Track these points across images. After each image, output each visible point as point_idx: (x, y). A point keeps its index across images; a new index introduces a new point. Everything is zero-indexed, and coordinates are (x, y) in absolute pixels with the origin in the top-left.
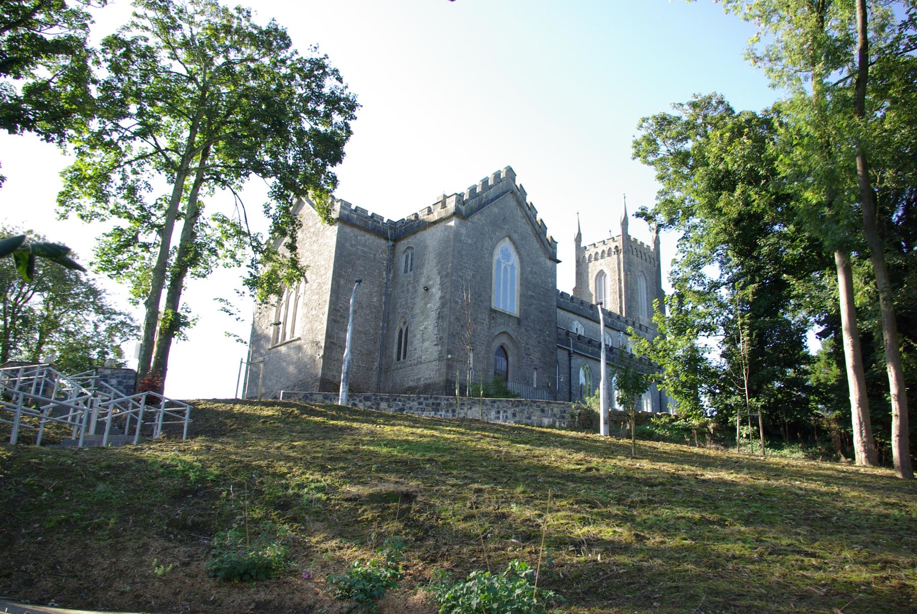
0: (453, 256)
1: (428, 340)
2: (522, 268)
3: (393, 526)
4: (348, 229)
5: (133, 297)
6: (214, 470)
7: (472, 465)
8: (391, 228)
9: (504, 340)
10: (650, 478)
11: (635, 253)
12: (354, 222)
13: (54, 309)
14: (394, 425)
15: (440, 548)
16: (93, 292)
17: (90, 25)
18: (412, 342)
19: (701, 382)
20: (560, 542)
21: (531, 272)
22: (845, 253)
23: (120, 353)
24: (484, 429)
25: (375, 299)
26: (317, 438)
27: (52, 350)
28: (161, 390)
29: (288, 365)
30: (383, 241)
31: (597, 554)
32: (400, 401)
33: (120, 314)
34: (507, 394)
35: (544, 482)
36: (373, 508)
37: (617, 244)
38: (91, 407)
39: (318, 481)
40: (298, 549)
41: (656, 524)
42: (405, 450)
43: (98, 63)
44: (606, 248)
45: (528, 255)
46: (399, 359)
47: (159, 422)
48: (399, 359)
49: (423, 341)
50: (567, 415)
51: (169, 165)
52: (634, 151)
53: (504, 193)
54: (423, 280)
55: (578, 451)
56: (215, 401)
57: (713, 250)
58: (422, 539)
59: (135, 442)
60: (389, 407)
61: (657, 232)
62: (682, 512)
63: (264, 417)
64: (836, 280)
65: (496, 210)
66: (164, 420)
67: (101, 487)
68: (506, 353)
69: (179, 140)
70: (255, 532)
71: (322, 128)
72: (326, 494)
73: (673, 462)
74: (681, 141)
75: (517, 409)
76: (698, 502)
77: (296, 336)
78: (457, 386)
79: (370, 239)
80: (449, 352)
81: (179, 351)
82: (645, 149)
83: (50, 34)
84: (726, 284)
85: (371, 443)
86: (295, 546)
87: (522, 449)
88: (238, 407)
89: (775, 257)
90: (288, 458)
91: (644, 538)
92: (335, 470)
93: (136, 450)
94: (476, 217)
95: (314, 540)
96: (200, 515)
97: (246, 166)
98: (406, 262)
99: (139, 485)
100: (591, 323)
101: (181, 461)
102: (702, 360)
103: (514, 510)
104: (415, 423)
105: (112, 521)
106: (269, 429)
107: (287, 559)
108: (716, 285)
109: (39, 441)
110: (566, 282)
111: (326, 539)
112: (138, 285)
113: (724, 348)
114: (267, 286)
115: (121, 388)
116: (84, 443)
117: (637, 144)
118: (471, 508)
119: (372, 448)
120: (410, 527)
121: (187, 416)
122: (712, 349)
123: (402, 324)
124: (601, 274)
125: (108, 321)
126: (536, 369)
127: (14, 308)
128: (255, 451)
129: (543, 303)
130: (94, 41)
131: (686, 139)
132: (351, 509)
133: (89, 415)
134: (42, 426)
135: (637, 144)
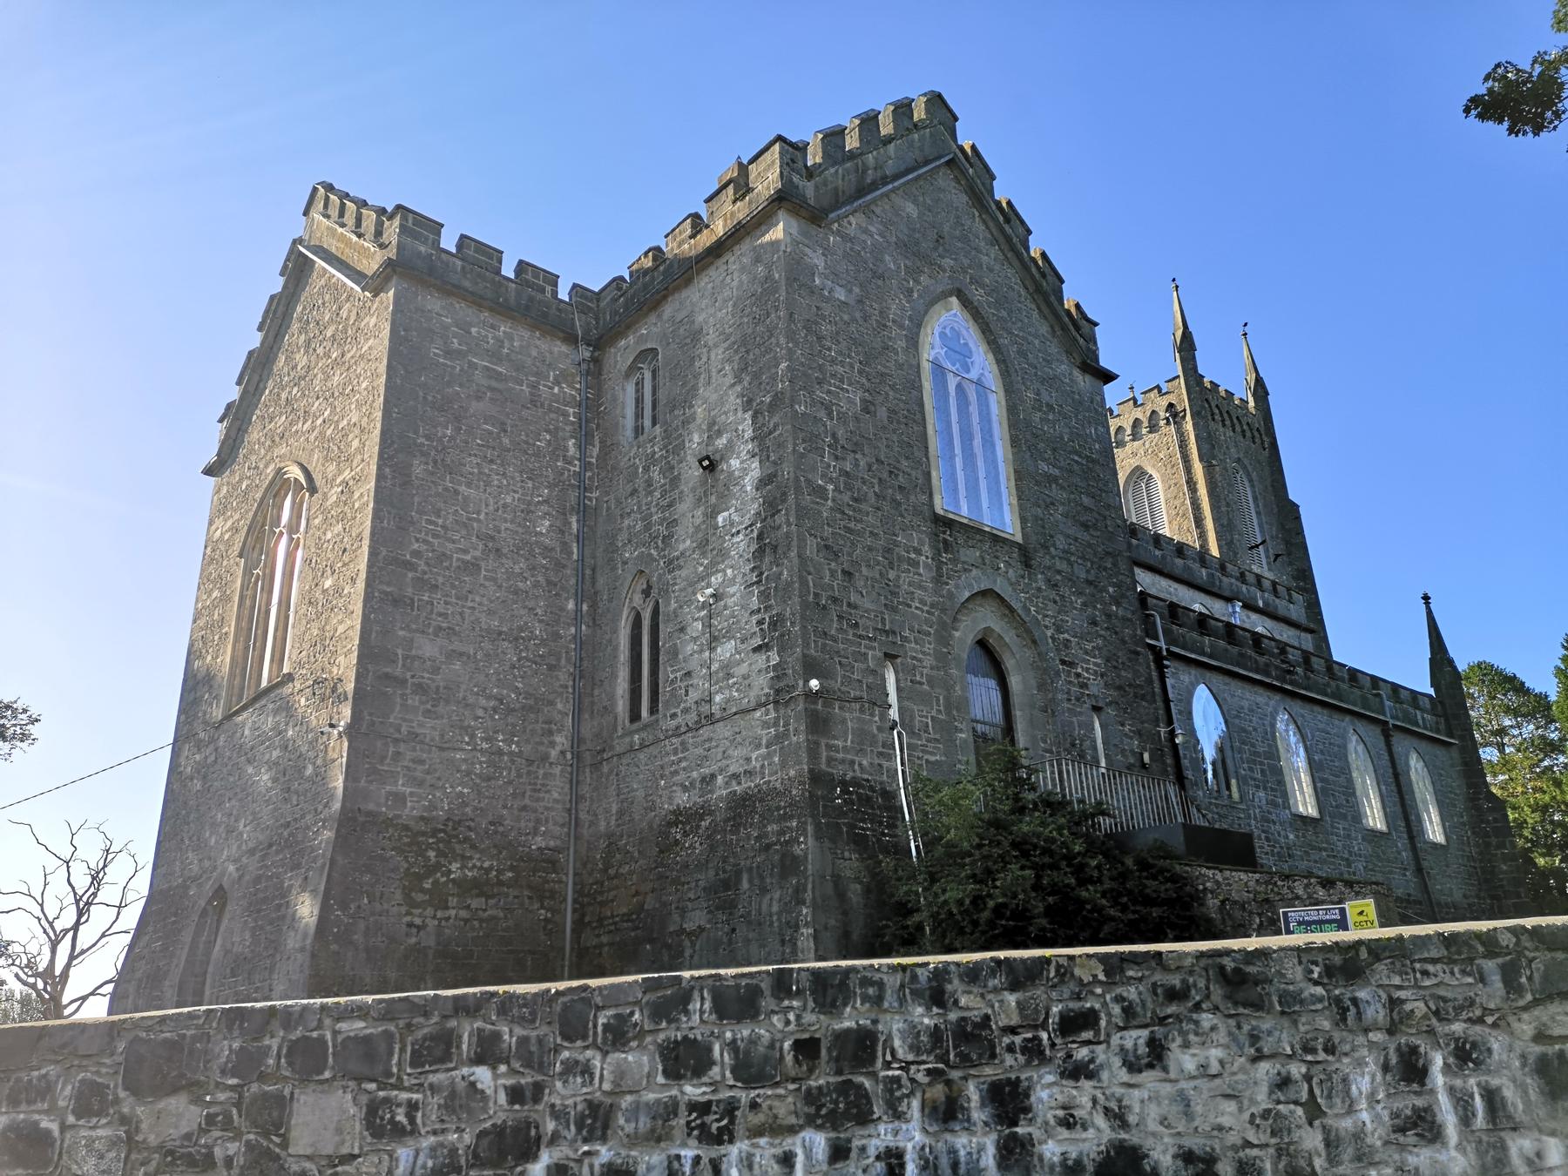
0: (791, 336)
1: (728, 635)
2: (1009, 390)
4: (433, 303)
8: (584, 310)
9: (987, 619)
11: (1217, 417)
18: (674, 652)
21: (1038, 405)
25: (544, 526)
30: (560, 348)
32: (487, 1052)
37: (1172, 398)
46: (635, 716)
48: (635, 716)
49: (714, 641)
54: (695, 442)
65: (911, 209)
80: (811, 669)
98: (639, 401)
123: (638, 599)
126: (1097, 709)
129: (1086, 500)
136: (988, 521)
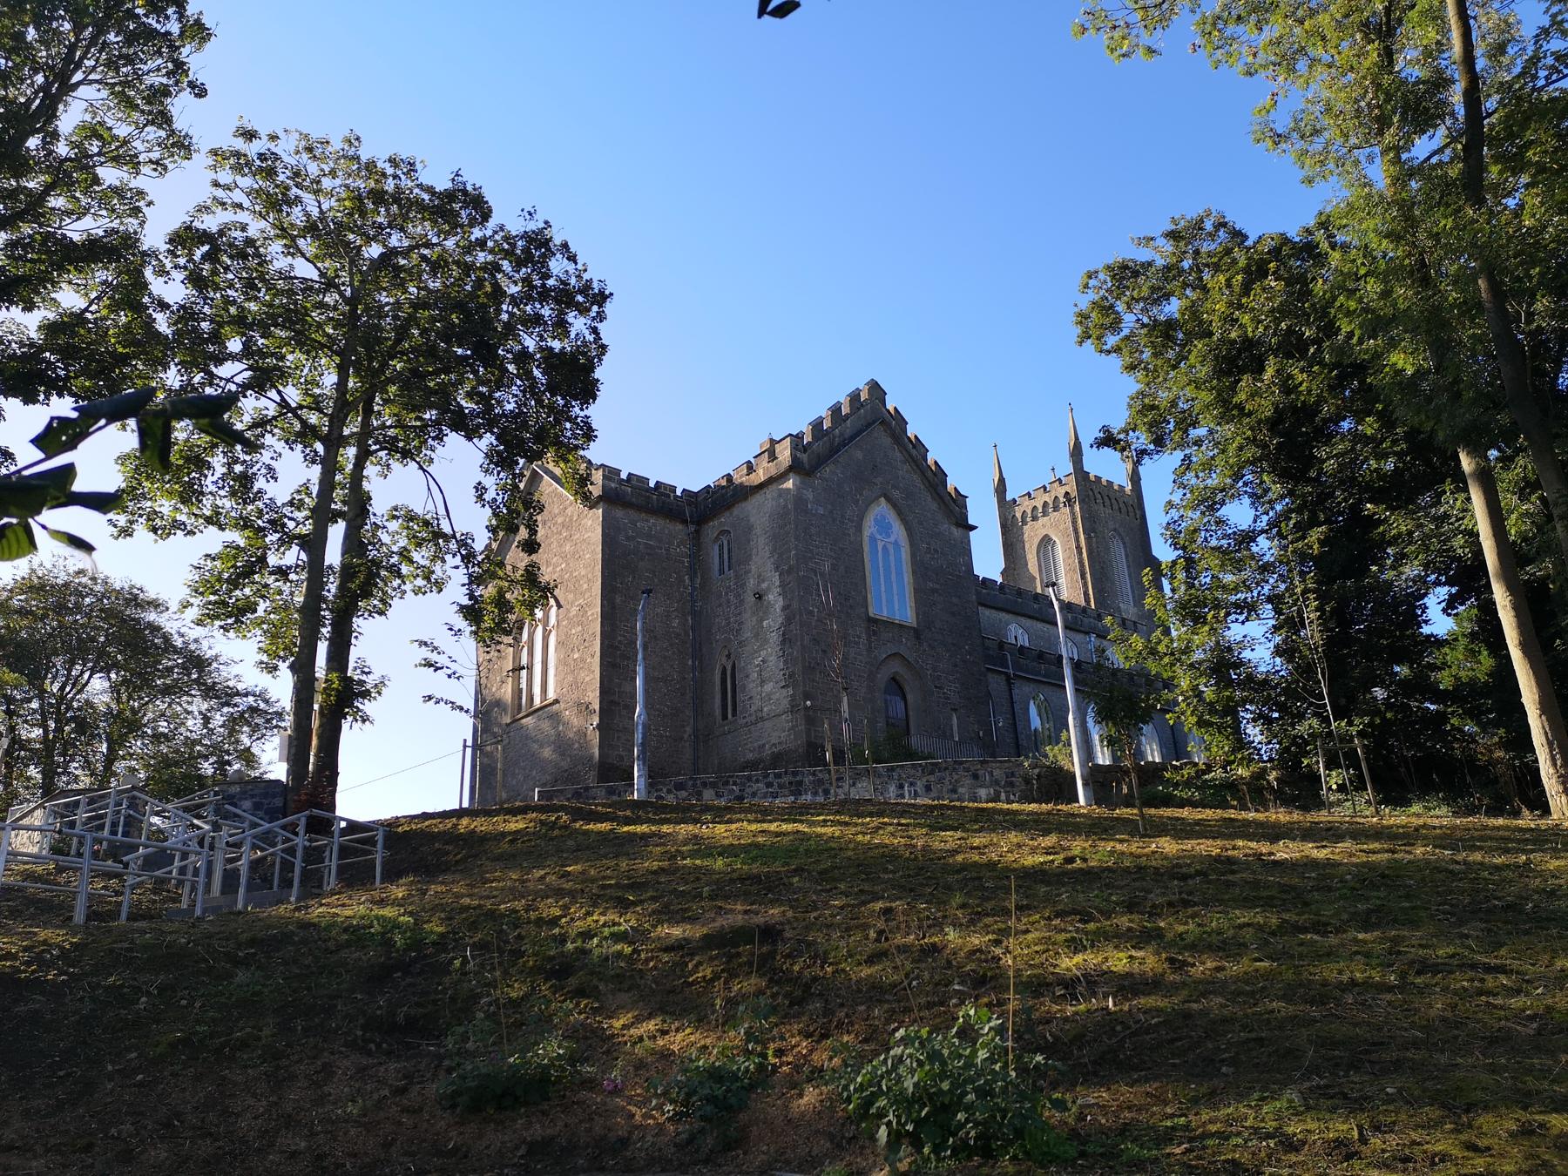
0: (797, 539)
2: (912, 544)
3: (749, 984)
4: (619, 513)
5: (265, 658)
6: (436, 927)
7: (869, 872)
9: (895, 667)
10: (1178, 866)
12: (627, 499)
13: (130, 697)
14: (730, 822)
15: (833, 1013)
16: (197, 663)
17: (145, 209)
18: (744, 687)
19: (1244, 701)
20: (1038, 986)
22: (1478, 451)
23: (248, 757)
24: (881, 814)
26: (605, 857)
27: (132, 766)
28: (332, 806)
29: (541, 746)
30: (680, 527)
31: (1105, 997)
32: (735, 784)
33: (246, 695)
34: (911, 755)
35: (989, 890)
36: (712, 959)
37: (1067, 488)
38: (212, 848)
39: (614, 924)
40: (593, 1043)
41: (1201, 939)
42: (754, 859)
43: (161, 272)
44: (1048, 498)
45: (921, 523)
46: (725, 717)
47: (333, 863)
48: (725, 717)
50: (1018, 780)
51: (307, 434)
52: (1079, 330)
53: (869, 425)
54: (751, 583)
55: (1046, 832)
56: (425, 816)
57: (1237, 476)
58: (800, 1002)
59: (293, 899)
60: (719, 796)
61: (1137, 463)
62: (1243, 916)
63: (510, 833)
64: (1469, 499)
65: (859, 455)
66: (340, 857)
67: (241, 976)
68: (901, 689)
69: (317, 391)
70: (521, 1023)
71: (556, 345)
72: (631, 943)
73: (1214, 838)
74: (1157, 302)
75: (932, 778)
76: (1272, 898)
77: (551, 695)
78: (828, 746)
79: (656, 524)
80: (807, 696)
81: (356, 745)
82: (1097, 324)
83: (76, 230)
84: (1266, 532)
85: (693, 854)
86: (586, 1038)
87: (948, 839)
88: (465, 821)
89: (1348, 477)
90: (559, 893)
91: (1184, 963)
92: (642, 902)
93: (298, 909)
94: (827, 470)
95: (618, 1024)
96: (418, 1005)
97: (437, 423)
99: (309, 966)
100: (1040, 625)
101: (377, 917)
102: (1239, 664)
103: (950, 938)
104: (765, 814)
105: (266, 1032)
106: (520, 852)
107: (572, 1059)
108: (1248, 537)
109: (124, 915)
110: (988, 561)
111: (638, 1020)
112: (273, 636)
113: (1278, 639)
114: (491, 619)
115: (261, 813)
116: (204, 911)
117: (1083, 317)
118: (878, 940)
119: (698, 862)
120: (778, 983)
121: (380, 845)
122: (1256, 642)
123: (724, 659)
124: (1046, 541)
125: (225, 710)
126: (955, 710)
127: (59, 704)
128: (500, 889)
129: (955, 600)
130: (154, 236)
131: (1167, 296)
132: (675, 964)
133: (210, 864)
134: (128, 891)
135: (1083, 317)
136: (897, 618)
